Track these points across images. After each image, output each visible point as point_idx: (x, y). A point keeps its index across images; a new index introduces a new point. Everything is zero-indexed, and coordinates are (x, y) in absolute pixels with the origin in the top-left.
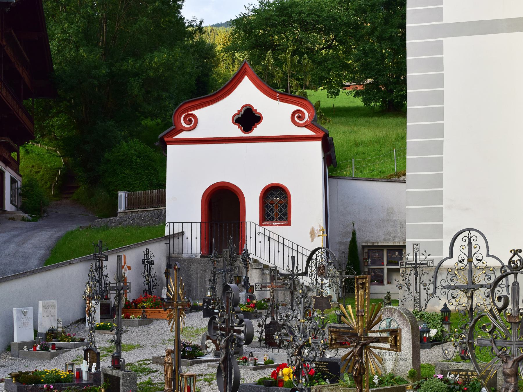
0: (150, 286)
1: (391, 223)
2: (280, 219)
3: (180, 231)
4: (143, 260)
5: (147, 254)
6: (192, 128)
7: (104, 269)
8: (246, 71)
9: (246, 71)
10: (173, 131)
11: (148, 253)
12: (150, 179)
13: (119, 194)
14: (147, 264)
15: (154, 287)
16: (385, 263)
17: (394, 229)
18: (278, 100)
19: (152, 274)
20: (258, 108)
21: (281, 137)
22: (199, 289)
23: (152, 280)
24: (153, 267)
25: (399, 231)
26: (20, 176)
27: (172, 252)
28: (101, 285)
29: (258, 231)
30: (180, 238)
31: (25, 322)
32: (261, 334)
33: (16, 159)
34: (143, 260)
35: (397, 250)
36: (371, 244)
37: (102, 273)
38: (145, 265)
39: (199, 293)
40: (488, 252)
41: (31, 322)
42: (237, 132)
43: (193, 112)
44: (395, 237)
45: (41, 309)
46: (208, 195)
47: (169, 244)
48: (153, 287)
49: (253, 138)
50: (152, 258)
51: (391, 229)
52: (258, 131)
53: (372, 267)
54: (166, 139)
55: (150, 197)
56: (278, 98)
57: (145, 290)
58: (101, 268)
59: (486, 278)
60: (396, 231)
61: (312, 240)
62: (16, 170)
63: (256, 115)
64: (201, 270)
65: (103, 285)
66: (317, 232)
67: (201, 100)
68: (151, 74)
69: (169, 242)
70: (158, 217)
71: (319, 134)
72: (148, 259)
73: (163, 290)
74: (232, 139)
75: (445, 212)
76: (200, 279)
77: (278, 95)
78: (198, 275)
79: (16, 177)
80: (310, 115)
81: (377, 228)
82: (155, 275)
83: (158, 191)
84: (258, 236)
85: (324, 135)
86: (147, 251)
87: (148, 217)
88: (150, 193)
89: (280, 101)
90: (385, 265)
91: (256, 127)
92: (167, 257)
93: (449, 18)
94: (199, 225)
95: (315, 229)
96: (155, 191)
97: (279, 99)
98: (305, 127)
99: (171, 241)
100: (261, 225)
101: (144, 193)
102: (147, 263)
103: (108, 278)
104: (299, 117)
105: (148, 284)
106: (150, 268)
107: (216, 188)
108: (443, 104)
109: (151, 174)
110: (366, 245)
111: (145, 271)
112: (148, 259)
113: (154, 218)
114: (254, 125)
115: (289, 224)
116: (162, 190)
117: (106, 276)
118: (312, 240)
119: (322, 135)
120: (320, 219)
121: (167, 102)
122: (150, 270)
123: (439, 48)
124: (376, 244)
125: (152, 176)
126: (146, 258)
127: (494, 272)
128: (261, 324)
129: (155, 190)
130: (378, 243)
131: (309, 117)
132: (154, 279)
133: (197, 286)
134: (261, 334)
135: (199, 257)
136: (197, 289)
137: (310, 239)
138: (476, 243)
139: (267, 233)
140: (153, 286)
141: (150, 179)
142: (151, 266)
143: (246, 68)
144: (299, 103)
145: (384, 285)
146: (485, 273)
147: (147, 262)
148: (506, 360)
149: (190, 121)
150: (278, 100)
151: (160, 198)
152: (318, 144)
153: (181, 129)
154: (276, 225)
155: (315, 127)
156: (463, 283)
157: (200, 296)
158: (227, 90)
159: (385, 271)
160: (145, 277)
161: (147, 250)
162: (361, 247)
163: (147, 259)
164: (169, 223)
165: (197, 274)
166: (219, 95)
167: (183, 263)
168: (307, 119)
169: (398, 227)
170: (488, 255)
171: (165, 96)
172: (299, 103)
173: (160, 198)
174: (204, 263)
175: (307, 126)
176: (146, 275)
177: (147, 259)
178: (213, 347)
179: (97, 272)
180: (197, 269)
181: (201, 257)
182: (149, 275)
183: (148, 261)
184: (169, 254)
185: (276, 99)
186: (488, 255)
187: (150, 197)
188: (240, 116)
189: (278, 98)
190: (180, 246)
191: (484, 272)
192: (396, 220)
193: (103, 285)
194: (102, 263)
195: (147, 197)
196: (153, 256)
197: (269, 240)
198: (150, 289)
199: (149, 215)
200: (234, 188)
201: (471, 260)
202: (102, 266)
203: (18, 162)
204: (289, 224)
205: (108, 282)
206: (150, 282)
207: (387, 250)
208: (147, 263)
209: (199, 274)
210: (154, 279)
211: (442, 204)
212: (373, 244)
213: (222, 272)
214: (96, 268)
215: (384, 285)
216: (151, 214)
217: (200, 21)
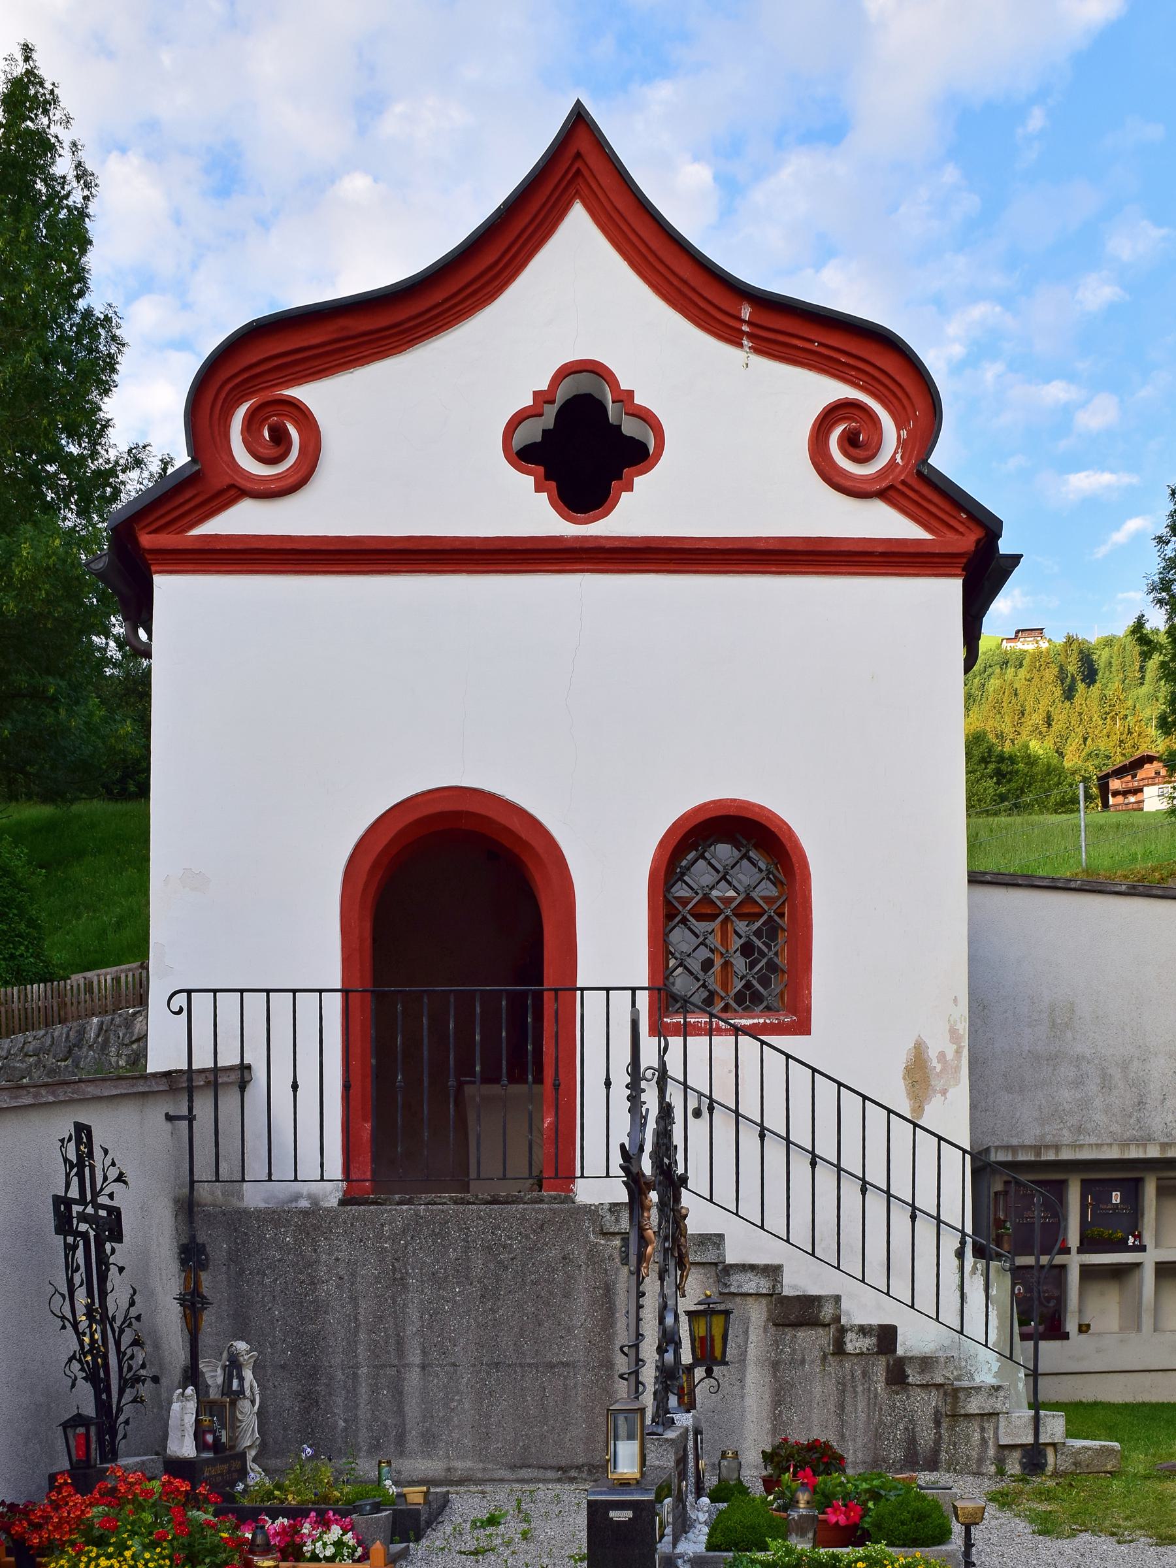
0: (108, 1389)
1: (1067, 1071)
2: (749, 999)
3: (229, 1058)
4: (57, 1200)
5: (80, 1164)
6: (290, 481)
8: (578, 172)
9: (578, 171)
10: (188, 494)
11: (91, 1154)
12: (12, 957)
14: (85, 1236)
15: (129, 1395)
16: (1074, 1240)
17: (1078, 1096)
18: (745, 342)
19: (117, 1302)
22: (363, 1390)
23: (118, 1343)
25: (1097, 1103)
27: (203, 1170)
29: (649, 1058)
30: (228, 1102)
34: (57, 1200)
35: (1116, 1184)
36: (1030, 1157)
38: (70, 1239)
39: (364, 1412)
43: (302, 393)
44: (1079, 1130)
46: (376, 865)
47: (191, 1119)
48: (121, 1392)
49: (617, 544)
50: (111, 1196)
51: (1066, 1096)
54: (147, 540)
55: (16, 1012)
56: (745, 328)
57: (78, 1420)
60: (1084, 1104)
64: (377, 1280)
66: (939, 1067)
67: (343, 322)
68: (7, 605)
69: (191, 1109)
70: (70, 1051)
71: (951, 536)
72: (89, 1198)
73: (176, 1406)
74: (506, 546)
76: (372, 1331)
77: (746, 312)
78: (356, 1306)
80: (904, 434)
81: (1009, 1089)
82: (134, 1312)
83: (49, 989)
85: (978, 542)
86: (79, 1142)
87: (26, 1055)
88: (15, 996)
89: (757, 351)
90: (1074, 1250)
92: (177, 1201)
95: (933, 1054)
96: (37, 989)
97: (750, 336)
98: (883, 495)
99: (203, 1108)
102: (83, 1227)
104: (850, 443)
106: (103, 1260)
107: (419, 822)
109: (17, 936)
110: (1010, 1158)
111: (70, 1281)
112: (89, 1198)
113: (50, 1060)
114: (548, 477)
116: (62, 983)
119: (967, 541)
120: (955, 1000)
121: (61, 710)
122: (103, 1279)
124: (1050, 1156)
125: (21, 944)
126: (74, 1193)
129: (35, 986)
130: (1057, 1148)
131: (902, 444)
132: (126, 1339)
133: (355, 1375)
135: (331, 1194)
136: (352, 1393)
141: (12, 957)
142: (108, 1246)
143: (579, 155)
144: (852, 362)
145: (1065, 1336)
147: (83, 1218)
149: (280, 438)
150: (745, 342)
151: (55, 1015)
153: (232, 486)
155: (936, 498)
157: (370, 1429)
159: (1074, 1276)
160: (75, 1325)
161: (83, 1132)
163: (82, 1201)
164: (189, 992)
165: (354, 1299)
166: (438, 296)
167: (275, 1239)
168: (893, 458)
169: (1093, 1087)
171: (56, 690)
172: (852, 362)
173: (55, 1015)
174: (393, 1239)
175: (891, 493)
176: (81, 1310)
177: (82, 1201)
180: (353, 1275)
181: (343, 1202)
182: (98, 1314)
183: (90, 1210)
184: (192, 1182)
185: (731, 336)
187: (16, 1012)
189: (745, 328)
190: (229, 1146)
192: (1083, 1057)
195: (6, 1011)
196: (120, 1178)
198: (103, 1406)
199: (30, 1048)
200: (515, 825)
207: (1083, 1181)
208: (83, 1227)
209: (363, 1304)
210: (126, 1339)
212: (1038, 1154)
215: (1065, 1336)
216: (35, 1043)
217: (162, 460)
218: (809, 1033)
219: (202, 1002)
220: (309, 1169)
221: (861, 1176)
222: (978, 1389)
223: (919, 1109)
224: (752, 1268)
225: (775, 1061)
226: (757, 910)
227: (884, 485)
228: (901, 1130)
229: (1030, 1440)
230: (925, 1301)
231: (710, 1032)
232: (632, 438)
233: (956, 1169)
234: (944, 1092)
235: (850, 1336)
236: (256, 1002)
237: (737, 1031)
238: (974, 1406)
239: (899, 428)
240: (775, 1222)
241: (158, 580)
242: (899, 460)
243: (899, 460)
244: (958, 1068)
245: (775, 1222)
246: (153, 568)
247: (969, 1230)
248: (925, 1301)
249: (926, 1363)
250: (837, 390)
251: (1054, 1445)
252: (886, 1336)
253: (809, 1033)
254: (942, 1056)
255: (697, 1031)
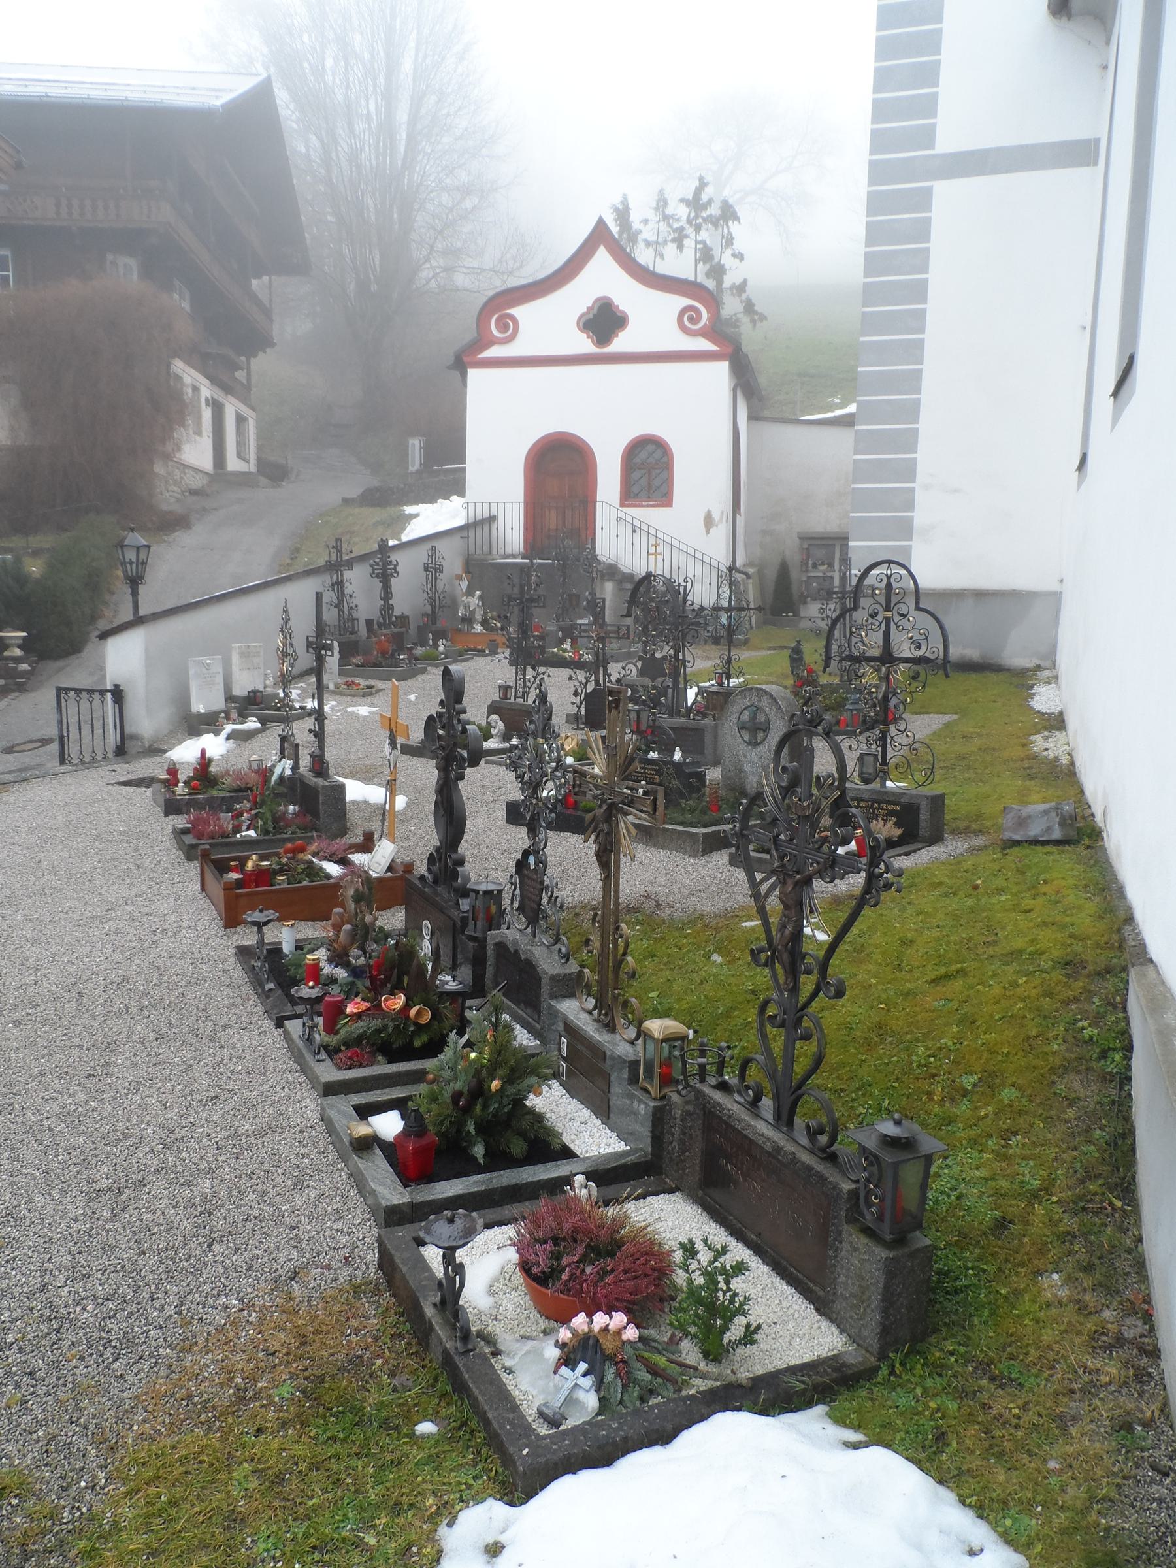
7: (347, 584)
13: (411, 442)
20: (622, 303)
24: (441, 576)
26: (253, 409)
28: (341, 611)
31: (209, 679)
32: (579, 707)
33: (245, 381)
37: (343, 592)
40: (917, 603)
41: (220, 680)
42: (585, 344)
43: (510, 311)
45: (235, 659)
52: (621, 343)
53: (812, 574)
58: (340, 584)
59: (913, 646)
61: (708, 532)
62: (245, 400)
63: (619, 314)
65: (346, 612)
75: (919, 497)
79: (245, 411)
91: (617, 336)
93: (948, 141)
94: (522, 505)
99: (472, 535)
100: (622, 505)
103: (353, 599)
104: (691, 319)
105: (431, 605)
106: (436, 578)
108: (925, 303)
115: (669, 504)
117: (351, 596)
118: (708, 532)
119: (730, 350)
123: (924, 200)
127: (927, 637)
128: (580, 691)
131: (709, 318)
134: (579, 707)
137: (703, 529)
138: (899, 585)
139: (629, 519)
140: (440, 607)
146: (912, 638)
148: (784, 879)
149: (506, 327)
152: (724, 367)
154: (648, 506)
156: (875, 653)
170: (918, 608)
178: (501, 725)
179: (333, 590)
182: (434, 587)
186: (918, 608)
188: (591, 316)
191: (910, 635)
193: (346, 612)
194: (342, 575)
197: (634, 531)
198: (433, 612)
201: (889, 614)
202: (342, 581)
203: (248, 387)
204: (669, 504)
205: (354, 606)
206: (435, 601)
211: (914, 482)
213: (518, 605)
214: (333, 585)
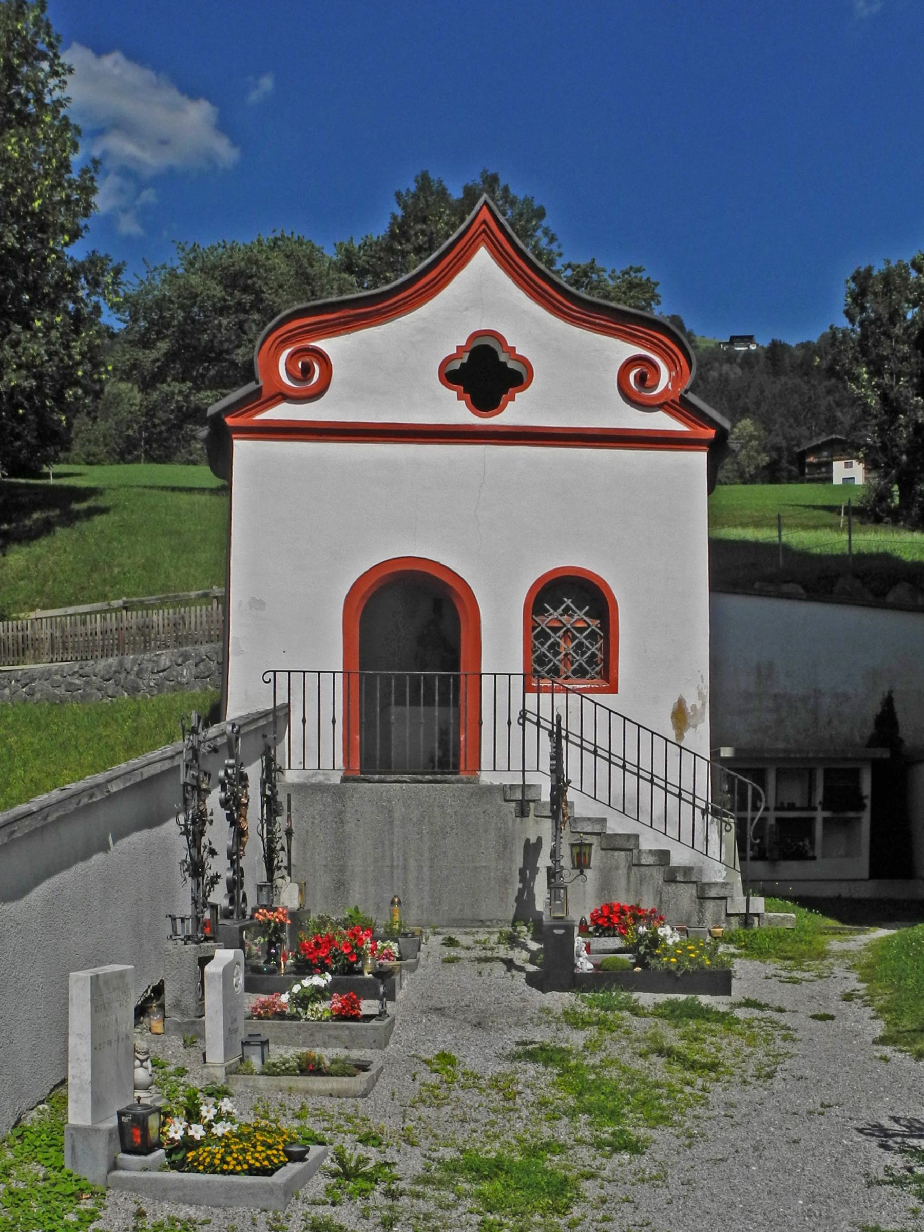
21: (560, 432)
43: (320, 344)
54: (229, 421)
80: (674, 374)
84: (516, 728)
94: (340, 678)
101: (15, 626)
114: (465, 392)
119: (711, 433)
135: (336, 779)
149: (307, 371)
158: (424, 287)
162: (871, 884)
164: (275, 672)
181: (345, 780)
218: (616, 692)
219: (282, 678)
220: (327, 763)
221: (527, 722)
222: (716, 884)
223: (680, 736)
224: (589, 819)
225: (588, 706)
226: (586, 625)
227: (662, 401)
228: (673, 749)
229: (744, 911)
230: (686, 837)
231: (552, 691)
232: (513, 369)
233: (703, 769)
234: (695, 726)
235: (644, 855)
236: (312, 678)
237: (567, 691)
238: (713, 893)
239: (670, 370)
240: (603, 795)
241: (235, 442)
242: (670, 387)
243: (670, 387)
244: (703, 714)
245: (603, 795)
246: (233, 436)
247: (710, 801)
248: (686, 837)
249: (687, 870)
250: (634, 350)
251: (757, 915)
252: (663, 856)
253: (616, 692)
254: (694, 707)
255: (546, 690)
